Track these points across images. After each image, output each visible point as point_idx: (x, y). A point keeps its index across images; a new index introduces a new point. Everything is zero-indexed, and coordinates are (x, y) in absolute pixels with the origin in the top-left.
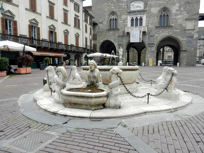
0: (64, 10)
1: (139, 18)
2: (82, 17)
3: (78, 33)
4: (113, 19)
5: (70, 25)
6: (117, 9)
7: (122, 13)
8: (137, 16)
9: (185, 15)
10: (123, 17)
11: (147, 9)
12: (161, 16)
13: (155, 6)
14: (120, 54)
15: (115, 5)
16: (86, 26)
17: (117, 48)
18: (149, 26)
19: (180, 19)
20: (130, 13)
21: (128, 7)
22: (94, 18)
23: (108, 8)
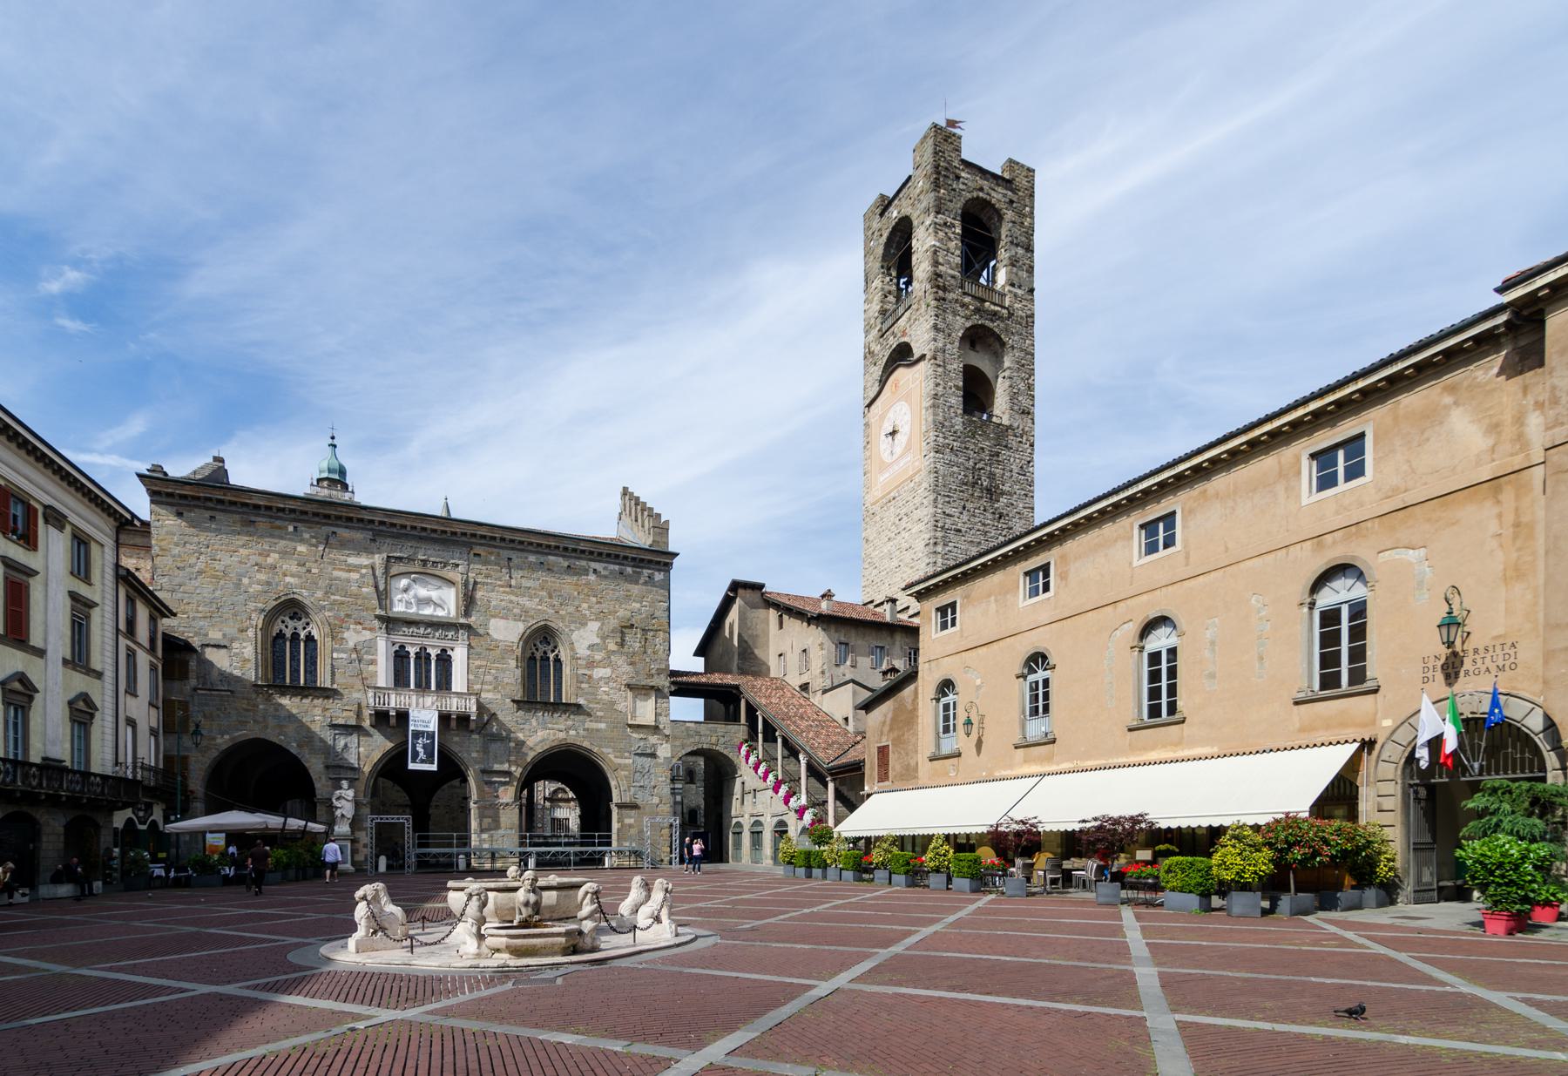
0: (74, 596)
1: (433, 652)
2: (109, 608)
3: (85, 697)
4: (295, 636)
5: (40, 653)
6: (319, 594)
7: (348, 616)
8: (426, 642)
9: (625, 671)
10: (353, 637)
11: (472, 620)
12: (532, 658)
13: (505, 614)
14: (338, 813)
15: (309, 571)
16: (131, 655)
17: (321, 786)
18: (483, 695)
19: (608, 680)
20: (391, 623)
21: (383, 596)
22: (175, 615)
23: (262, 577)
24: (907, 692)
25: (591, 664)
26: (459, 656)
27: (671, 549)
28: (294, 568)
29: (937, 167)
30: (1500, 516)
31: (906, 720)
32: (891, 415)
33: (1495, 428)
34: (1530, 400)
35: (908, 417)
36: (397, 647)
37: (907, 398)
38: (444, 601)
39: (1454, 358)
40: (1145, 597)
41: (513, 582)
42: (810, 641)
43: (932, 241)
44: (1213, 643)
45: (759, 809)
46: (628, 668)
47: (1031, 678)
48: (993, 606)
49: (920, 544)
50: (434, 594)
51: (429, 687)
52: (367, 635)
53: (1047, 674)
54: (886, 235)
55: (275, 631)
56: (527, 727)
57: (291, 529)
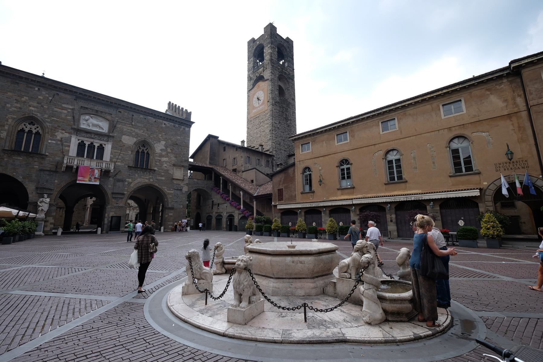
1: (97, 145)
7: (59, 126)
12: (138, 152)
13: (130, 134)
15: (42, 106)
17: (32, 196)
19: (166, 162)
20: (78, 131)
21: (75, 120)
23: (18, 105)
24: (290, 170)
25: (161, 156)
26: (108, 148)
27: (192, 120)
28: (35, 104)
29: (271, 33)
30: (513, 124)
31: (292, 179)
32: (257, 94)
33: (506, 101)
34: (516, 94)
35: (263, 95)
36: (80, 141)
37: (263, 90)
38: (104, 126)
39: (500, 77)
40: (407, 139)
41: (133, 123)
42: (237, 155)
43: (270, 51)
44: (414, 158)
45: (221, 210)
46: (174, 159)
47: (342, 167)
48: (325, 144)
49: (268, 131)
50: (100, 124)
51: (93, 158)
52: (67, 135)
53: (348, 166)
54: (255, 48)
55: (20, 128)
56: (133, 177)
57: (37, 89)
